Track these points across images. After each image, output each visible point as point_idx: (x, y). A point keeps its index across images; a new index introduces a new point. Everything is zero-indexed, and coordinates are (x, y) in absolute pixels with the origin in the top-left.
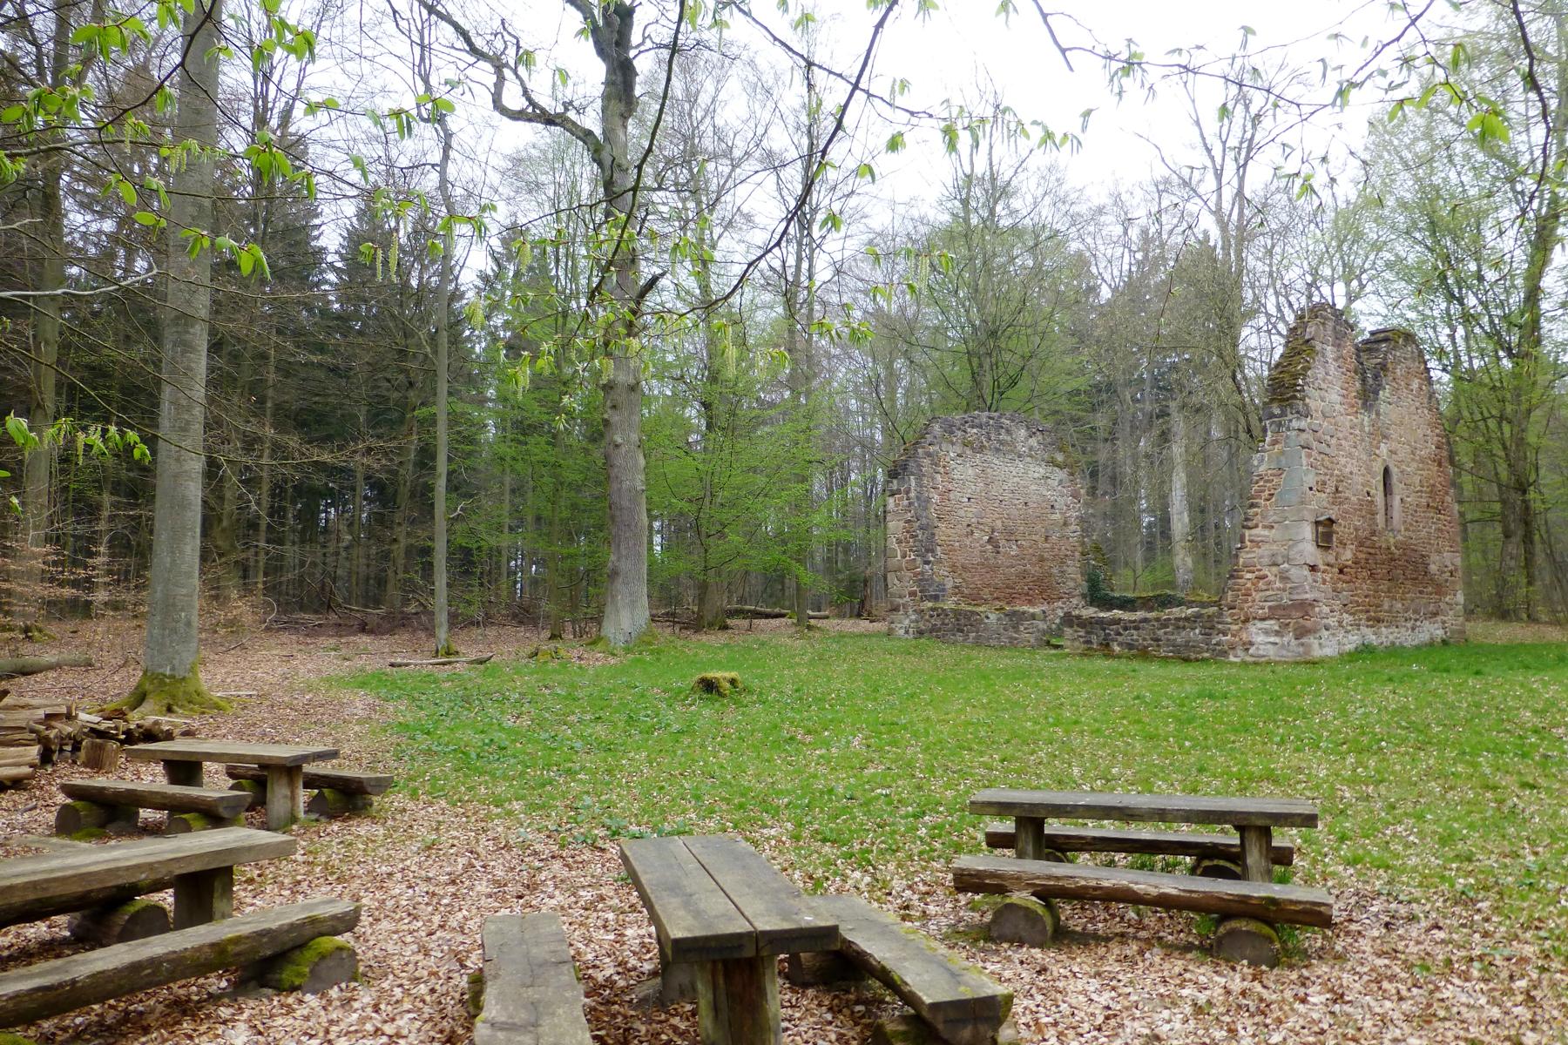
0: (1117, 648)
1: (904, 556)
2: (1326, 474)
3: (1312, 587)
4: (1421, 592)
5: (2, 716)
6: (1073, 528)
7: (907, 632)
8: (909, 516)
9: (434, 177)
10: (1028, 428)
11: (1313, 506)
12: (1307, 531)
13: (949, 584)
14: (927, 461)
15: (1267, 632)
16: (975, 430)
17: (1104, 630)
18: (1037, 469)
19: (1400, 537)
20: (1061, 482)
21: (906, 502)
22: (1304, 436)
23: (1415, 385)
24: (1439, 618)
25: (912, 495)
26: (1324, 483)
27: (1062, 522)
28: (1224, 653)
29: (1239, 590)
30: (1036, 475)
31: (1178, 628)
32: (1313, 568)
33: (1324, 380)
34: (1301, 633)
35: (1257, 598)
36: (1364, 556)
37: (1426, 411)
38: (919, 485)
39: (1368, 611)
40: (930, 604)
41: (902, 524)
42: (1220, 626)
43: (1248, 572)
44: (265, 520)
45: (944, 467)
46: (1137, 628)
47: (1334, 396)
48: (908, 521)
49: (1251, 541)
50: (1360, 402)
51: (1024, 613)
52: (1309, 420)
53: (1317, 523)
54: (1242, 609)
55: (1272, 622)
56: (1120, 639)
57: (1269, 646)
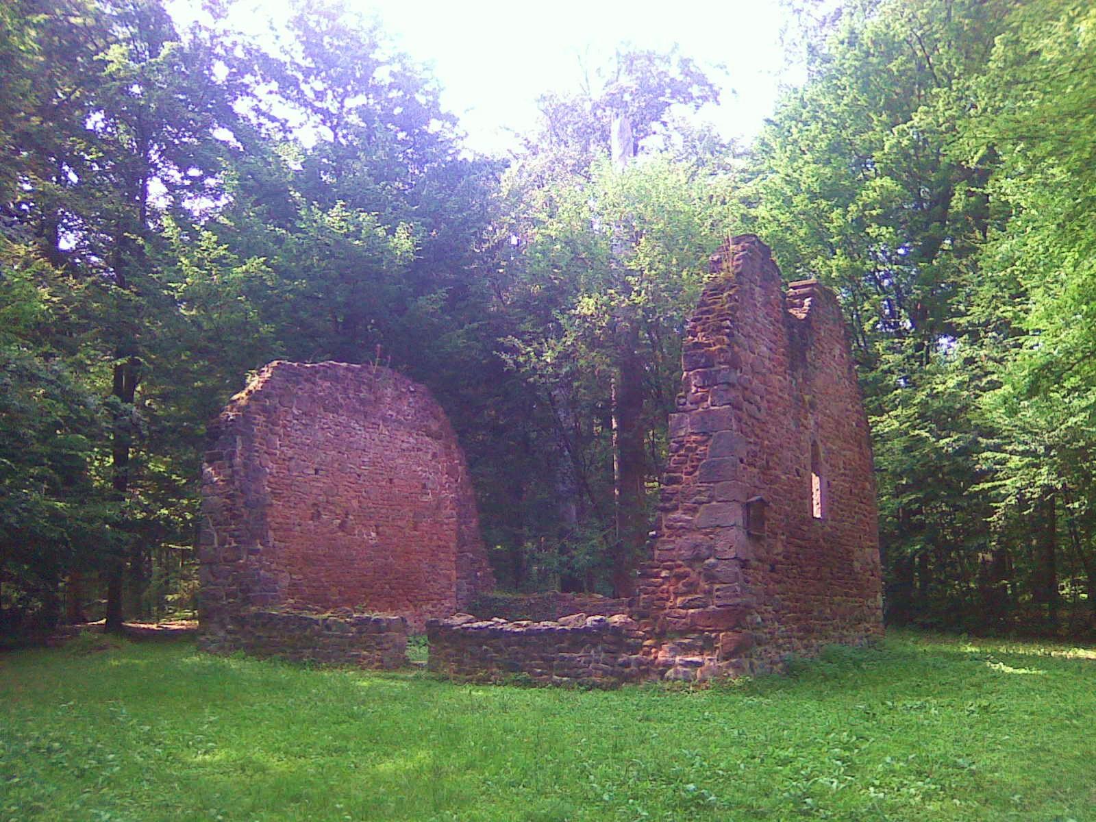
1: (222, 544)
3: (743, 588)
4: (846, 594)
5: (1094, 700)
6: (448, 511)
12: (735, 516)
13: (284, 582)
20: (434, 455)
30: (405, 446)
38: (249, 448)
39: (799, 619)
43: (665, 568)
45: (285, 427)
49: (668, 527)
53: (748, 506)
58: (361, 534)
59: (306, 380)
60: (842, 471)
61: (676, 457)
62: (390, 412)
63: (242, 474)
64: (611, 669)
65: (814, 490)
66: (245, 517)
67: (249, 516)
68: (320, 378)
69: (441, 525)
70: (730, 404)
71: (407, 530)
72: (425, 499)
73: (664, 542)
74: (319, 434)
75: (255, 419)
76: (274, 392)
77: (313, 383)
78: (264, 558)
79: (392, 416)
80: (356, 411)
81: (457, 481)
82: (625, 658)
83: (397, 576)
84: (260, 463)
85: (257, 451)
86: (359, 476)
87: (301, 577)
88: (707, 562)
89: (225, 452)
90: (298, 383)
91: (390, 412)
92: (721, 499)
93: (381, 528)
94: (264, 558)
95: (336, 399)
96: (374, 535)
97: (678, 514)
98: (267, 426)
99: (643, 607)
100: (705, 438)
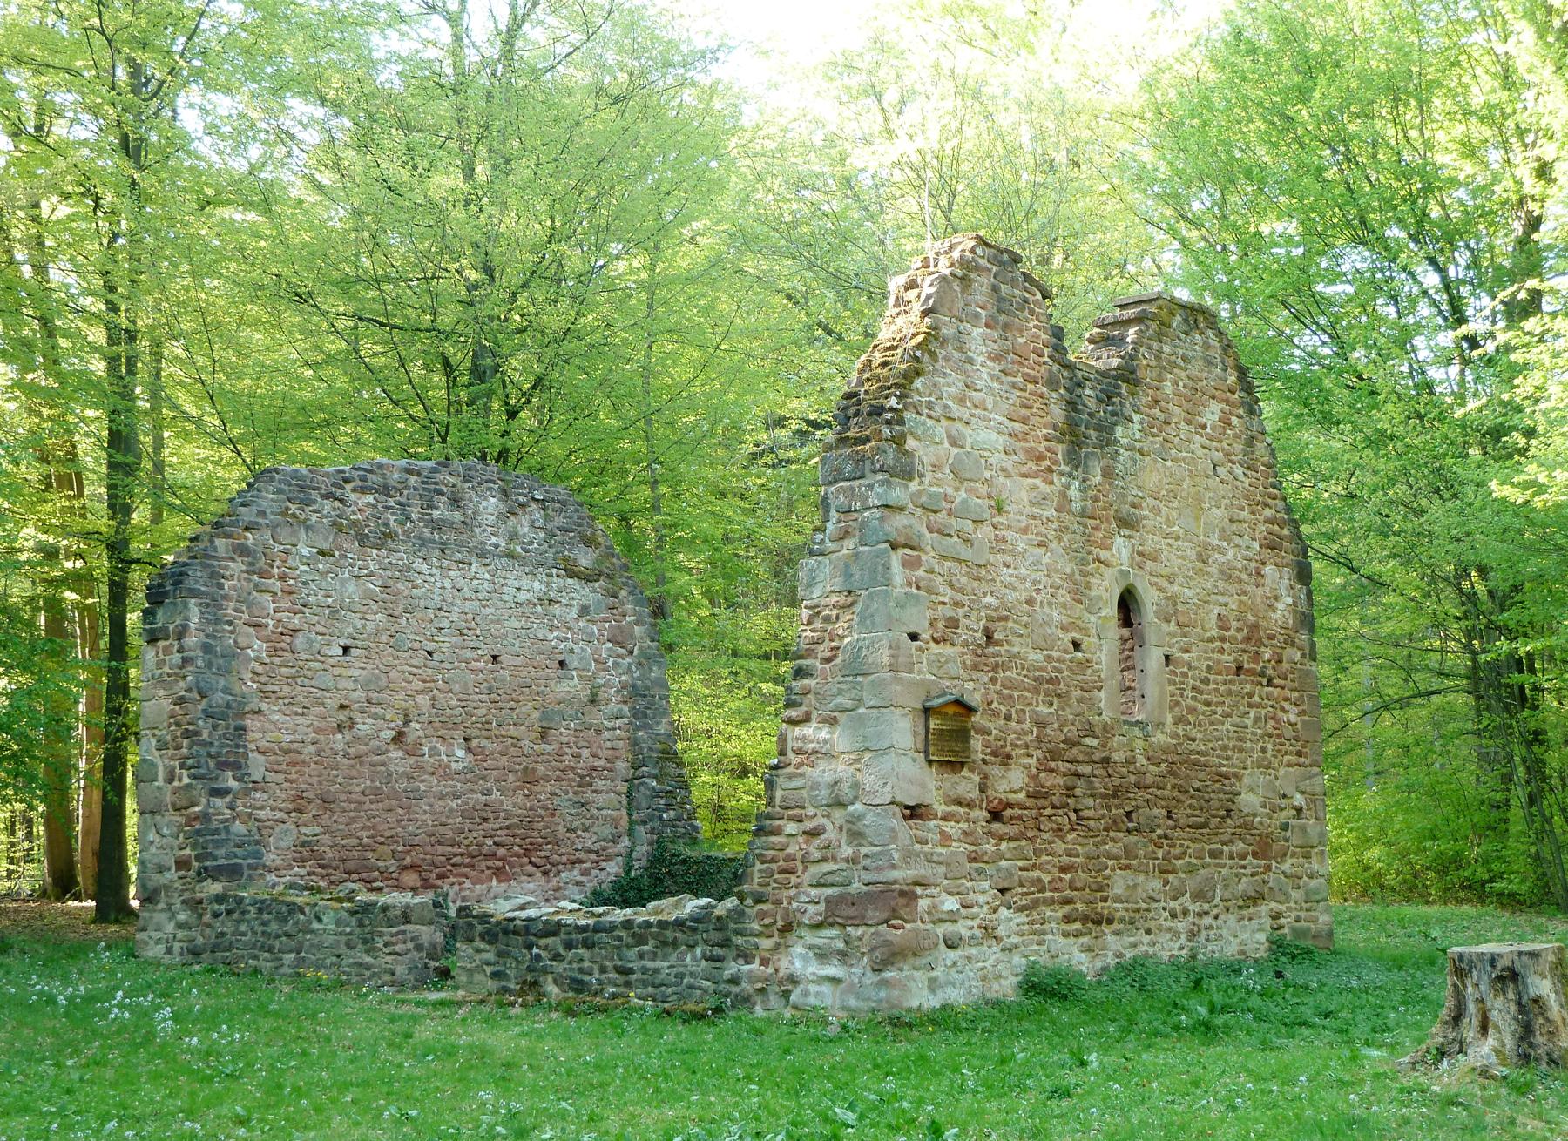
0: (552, 989)
1: (170, 780)
2: (957, 604)
4: (1215, 854)
6: (613, 707)
7: (169, 951)
8: (180, 688)
9: (675, 113)
10: (504, 492)
11: (923, 673)
12: (903, 731)
14: (237, 566)
15: (822, 955)
16: (370, 499)
17: (529, 947)
18: (524, 583)
19: (1160, 738)
20: (584, 610)
21: (177, 658)
22: (900, 520)
23: (1212, 413)
24: (1264, 908)
25: (192, 640)
26: (953, 623)
27: (584, 696)
28: (744, 1001)
29: (774, 860)
30: (523, 596)
31: (664, 943)
32: (914, 812)
33: (961, 401)
34: (888, 957)
35: (807, 877)
36: (1061, 780)
37: (1239, 471)
40: (216, 888)
41: (167, 705)
42: (739, 941)
43: (791, 819)
44: (1045, 652)
45: (283, 578)
46: (590, 945)
47: (988, 436)
48: (180, 701)
50: (1061, 449)
51: (385, 908)
52: (914, 486)
54: (778, 903)
55: (834, 932)
56: (559, 967)
57: (826, 988)
58: (434, 752)
59: (326, 496)
60: (1215, 632)
61: (809, 633)
62: (494, 539)
63: (200, 663)
64: (713, 986)
65: (128, 812)
66: (205, 735)
67: (210, 735)
68: (354, 490)
69: (599, 732)
70: (887, 541)
71: (526, 743)
72: (564, 686)
73: (790, 777)
74: (351, 587)
75: (226, 567)
76: (261, 521)
77: (341, 501)
78: (239, 802)
79: (497, 546)
80: (424, 542)
81: (631, 653)
82: (734, 971)
83: (508, 822)
84: (235, 642)
85: (230, 623)
86: (430, 653)
87: (318, 829)
88: (851, 808)
89: (171, 627)
90: (308, 502)
91: (494, 539)
92: (872, 703)
93: (475, 743)
94: (239, 802)
95: (386, 525)
96: (460, 753)
97: (808, 730)
98: (250, 580)
99: (760, 884)
100: (850, 599)
